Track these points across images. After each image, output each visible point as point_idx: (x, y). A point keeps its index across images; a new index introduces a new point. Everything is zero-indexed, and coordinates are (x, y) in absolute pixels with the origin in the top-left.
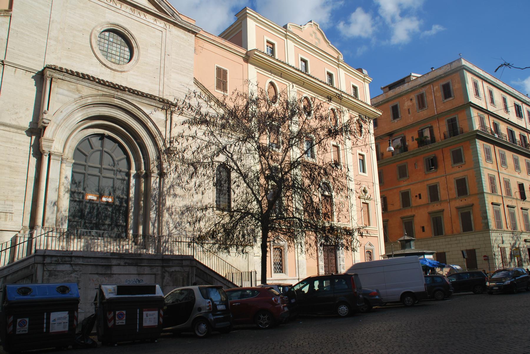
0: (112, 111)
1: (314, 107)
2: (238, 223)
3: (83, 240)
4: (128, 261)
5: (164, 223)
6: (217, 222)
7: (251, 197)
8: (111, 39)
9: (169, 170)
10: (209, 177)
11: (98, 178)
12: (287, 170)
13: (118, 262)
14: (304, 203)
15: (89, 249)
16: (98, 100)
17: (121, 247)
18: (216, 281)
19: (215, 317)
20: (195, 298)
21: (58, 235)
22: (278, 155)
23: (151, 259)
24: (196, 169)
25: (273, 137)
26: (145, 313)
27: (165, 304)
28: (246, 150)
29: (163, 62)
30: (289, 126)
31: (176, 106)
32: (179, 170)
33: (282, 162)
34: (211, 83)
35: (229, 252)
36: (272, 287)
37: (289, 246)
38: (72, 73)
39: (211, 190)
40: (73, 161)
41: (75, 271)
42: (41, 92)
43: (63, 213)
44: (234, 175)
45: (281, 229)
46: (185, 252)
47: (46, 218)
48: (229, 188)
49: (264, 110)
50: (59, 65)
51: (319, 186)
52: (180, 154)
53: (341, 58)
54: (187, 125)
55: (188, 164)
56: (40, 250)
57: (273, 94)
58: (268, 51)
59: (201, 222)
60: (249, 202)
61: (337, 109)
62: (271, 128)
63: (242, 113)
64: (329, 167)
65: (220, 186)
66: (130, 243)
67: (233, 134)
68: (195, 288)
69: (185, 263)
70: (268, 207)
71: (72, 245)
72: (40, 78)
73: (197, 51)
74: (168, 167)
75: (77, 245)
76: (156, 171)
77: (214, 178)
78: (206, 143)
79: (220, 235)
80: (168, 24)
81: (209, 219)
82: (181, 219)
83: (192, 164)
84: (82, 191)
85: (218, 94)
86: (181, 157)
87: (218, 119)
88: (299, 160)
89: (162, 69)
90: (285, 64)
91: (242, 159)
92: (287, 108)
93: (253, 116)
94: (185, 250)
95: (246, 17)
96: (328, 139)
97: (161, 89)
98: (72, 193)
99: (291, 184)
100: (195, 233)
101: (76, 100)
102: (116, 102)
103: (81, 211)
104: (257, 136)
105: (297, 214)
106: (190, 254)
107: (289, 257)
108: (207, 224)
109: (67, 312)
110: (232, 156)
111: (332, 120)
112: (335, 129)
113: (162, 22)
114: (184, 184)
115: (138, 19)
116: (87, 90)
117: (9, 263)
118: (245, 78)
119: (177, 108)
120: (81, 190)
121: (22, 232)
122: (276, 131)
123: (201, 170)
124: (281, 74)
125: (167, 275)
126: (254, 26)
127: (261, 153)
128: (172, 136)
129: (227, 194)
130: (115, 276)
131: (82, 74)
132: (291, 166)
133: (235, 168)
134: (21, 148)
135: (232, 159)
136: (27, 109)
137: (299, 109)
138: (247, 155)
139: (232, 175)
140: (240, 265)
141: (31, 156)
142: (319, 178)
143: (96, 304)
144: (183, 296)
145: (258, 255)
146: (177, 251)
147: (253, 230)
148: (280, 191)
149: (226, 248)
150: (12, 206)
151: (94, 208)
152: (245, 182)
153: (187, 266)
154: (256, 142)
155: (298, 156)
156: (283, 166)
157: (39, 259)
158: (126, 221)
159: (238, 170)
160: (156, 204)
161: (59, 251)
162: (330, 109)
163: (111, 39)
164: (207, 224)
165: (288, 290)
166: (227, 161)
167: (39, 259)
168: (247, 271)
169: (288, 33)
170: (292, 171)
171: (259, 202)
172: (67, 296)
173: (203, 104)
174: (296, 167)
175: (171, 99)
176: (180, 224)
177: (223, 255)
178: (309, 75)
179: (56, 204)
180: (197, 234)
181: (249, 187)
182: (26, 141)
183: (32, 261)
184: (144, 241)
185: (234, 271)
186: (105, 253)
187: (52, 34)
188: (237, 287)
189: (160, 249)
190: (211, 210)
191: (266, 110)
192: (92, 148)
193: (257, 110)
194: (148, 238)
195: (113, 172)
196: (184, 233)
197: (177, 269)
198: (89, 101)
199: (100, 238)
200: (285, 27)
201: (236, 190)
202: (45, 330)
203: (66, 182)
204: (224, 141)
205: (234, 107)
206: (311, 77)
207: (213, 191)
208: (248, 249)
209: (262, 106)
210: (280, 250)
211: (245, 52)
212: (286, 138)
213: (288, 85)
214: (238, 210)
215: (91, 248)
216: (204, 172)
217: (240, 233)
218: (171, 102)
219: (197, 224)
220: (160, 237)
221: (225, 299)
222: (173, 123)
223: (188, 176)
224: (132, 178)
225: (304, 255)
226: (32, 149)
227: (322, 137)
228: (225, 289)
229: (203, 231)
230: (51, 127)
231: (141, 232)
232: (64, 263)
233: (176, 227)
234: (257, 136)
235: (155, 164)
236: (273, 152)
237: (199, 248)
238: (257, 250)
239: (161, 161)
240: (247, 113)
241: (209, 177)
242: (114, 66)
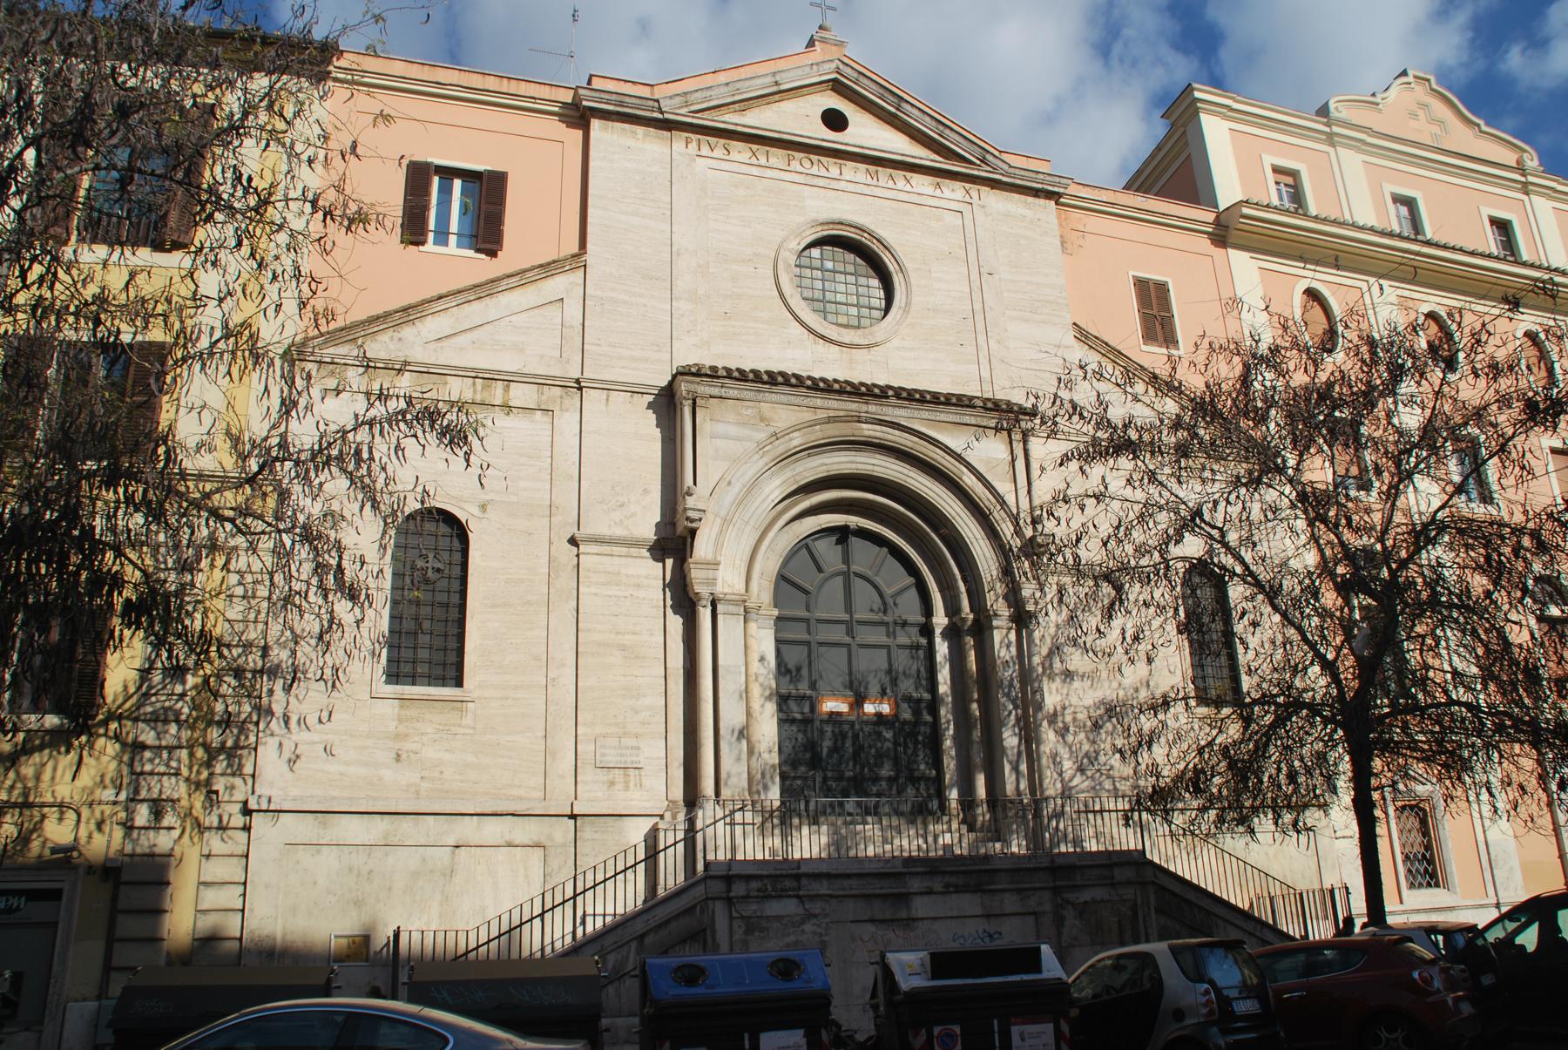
0: (859, 459)
1: (1463, 339)
2: (1269, 740)
3: (824, 828)
4: (953, 880)
5: (1044, 761)
6: (1203, 743)
7: (1300, 653)
8: (829, 265)
9: (1042, 604)
10: (1161, 609)
11: (885, 651)
12: (1403, 554)
13: (926, 884)
14: (1480, 651)
15: (843, 851)
16: (819, 434)
17: (930, 839)
18: (1220, 923)
19: (1231, 1039)
20: (1160, 981)
21: (758, 820)
22: (1368, 511)
23: (1019, 870)
24: (1119, 588)
25: (1343, 458)
26: (1015, 1030)
27: (1073, 1003)
28: (1264, 511)
29: (977, 296)
30: (1389, 415)
31: (1035, 415)
32: (1071, 600)
33: (1385, 531)
34: (1125, 329)
35: (1252, 831)
36: (1406, 934)
37: (1449, 798)
38: (742, 376)
39: (1173, 648)
40: (776, 612)
41: (810, 916)
42: (674, 440)
43: (766, 756)
44: (1237, 592)
45: (1413, 745)
46: (1116, 841)
47: (723, 775)
48: (1229, 636)
49: (1299, 379)
50: (379, 311)
51: (1525, 591)
52: (1068, 552)
53: (1532, 162)
54: (1074, 465)
55: (1095, 578)
56: (717, 863)
57: (1321, 324)
58: (1281, 199)
59: (1155, 747)
60: (1295, 671)
61: (1547, 331)
62: (1331, 431)
63: (1234, 401)
64: (1548, 525)
65: (1199, 631)
66: (955, 825)
67: (1216, 467)
68: (1159, 948)
69: (1120, 874)
70: (1359, 677)
71: (797, 843)
72: (667, 403)
73: (1068, 245)
74: (1038, 594)
75: (809, 844)
76: (1003, 610)
77: (1176, 610)
78: (1137, 508)
79: (1217, 780)
80: (974, 189)
81: (1179, 736)
82: (1094, 742)
83: (1107, 577)
84: (808, 692)
85: (1153, 357)
86: (1071, 561)
87: (1165, 432)
88: (1440, 515)
89: (979, 317)
90: (1343, 224)
91: (1255, 539)
92: (1375, 360)
93: (1270, 403)
94: (1116, 835)
95: (1196, 112)
96: (1531, 434)
97: (986, 374)
98: (783, 700)
99: (1424, 595)
100: (1142, 783)
101: (761, 447)
102: (867, 433)
103: (812, 746)
104: (1291, 463)
105: (1461, 690)
106: (1132, 847)
107: (1457, 831)
108: (1175, 752)
109: (801, 1032)
110: (1223, 535)
111: (1535, 370)
112: (1547, 398)
113: (958, 185)
114: (1089, 640)
115: (890, 194)
116: (785, 412)
117: (645, 901)
118: (1225, 295)
119: (1038, 421)
120: (804, 688)
121: (668, 816)
122: (1347, 435)
123: (1134, 591)
124: (1337, 258)
125: (1069, 914)
126: (1227, 134)
127: (1312, 515)
128: (1036, 502)
129: (1224, 652)
131: (767, 372)
132: (1417, 538)
133: (1239, 570)
134: (642, 593)
135: (1226, 545)
136: (646, 491)
137: (1414, 357)
138: (1270, 525)
139: (1231, 593)
140: (1296, 867)
141: (669, 611)
142: (1520, 565)
143: (875, 1007)
144: (1125, 976)
145: (1348, 833)
146: (1094, 841)
147: (1321, 757)
148: (1393, 624)
149: (1243, 820)
150: (638, 748)
151: (844, 736)
152: (1275, 608)
153: (1128, 883)
154: (1291, 481)
155: (1436, 503)
156: (1389, 543)
157: (717, 888)
158: (937, 763)
159: (1250, 577)
160: (1016, 707)
161: (764, 861)
162: (1520, 334)
163: (829, 265)
164: (1175, 752)
165: (1464, 944)
166: (1211, 552)
167: (717, 888)
168: (1317, 886)
169: (1336, 129)
170: (1424, 554)
171: (1329, 667)
172: (796, 985)
173: (1113, 395)
174: (1433, 541)
175: (1018, 398)
176: (1092, 758)
177: (1234, 842)
178: (1428, 243)
179: (743, 733)
180: (1147, 783)
181: (1292, 624)
182: (652, 574)
183: (699, 891)
184: (994, 819)
185: (1276, 890)
186: (888, 861)
187: (680, 285)
188: (1293, 939)
189: (1043, 837)
190: (1180, 706)
191: (1308, 379)
192: (820, 570)
193: (1280, 383)
194: (1004, 809)
195: (883, 629)
196: (1108, 785)
197: (1099, 893)
198: (795, 443)
199: (869, 819)
200: (1323, 111)
201: (1250, 639)
203: (764, 671)
204: (1191, 493)
205: (1207, 386)
206: (1437, 246)
207: (1178, 647)
208: (1312, 816)
209: (1292, 368)
210: (1421, 816)
211: (1211, 217)
212: (1386, 452)
213: (1365, 289)
214: (1266, 699)
215: (848, 849)
216: (1146, 596)
217: (1279, 770)
218: (1020, 406)
219: (1145, 755)
220: (1038, 803)
221: (1255, 981)
222: (1035, 466)
223: (1099, 613)
224: (938, 639)
225: (1503, 823)
226: (668, 594)
227: (1510, 431)
228: (1251, 948)
229: (1165, 773)
230: (707, 530)
231: (981, 792)
232: (781, 895)
233: (1081, 770)
234: (1291, 463)
235: (999, 591)
236: (1350, 505)
237: (1158, 826)
238: (1341, 818)
239: (1013, 581)
240: (1249, 400)
241: (1161, 609)
242: (848, 336)
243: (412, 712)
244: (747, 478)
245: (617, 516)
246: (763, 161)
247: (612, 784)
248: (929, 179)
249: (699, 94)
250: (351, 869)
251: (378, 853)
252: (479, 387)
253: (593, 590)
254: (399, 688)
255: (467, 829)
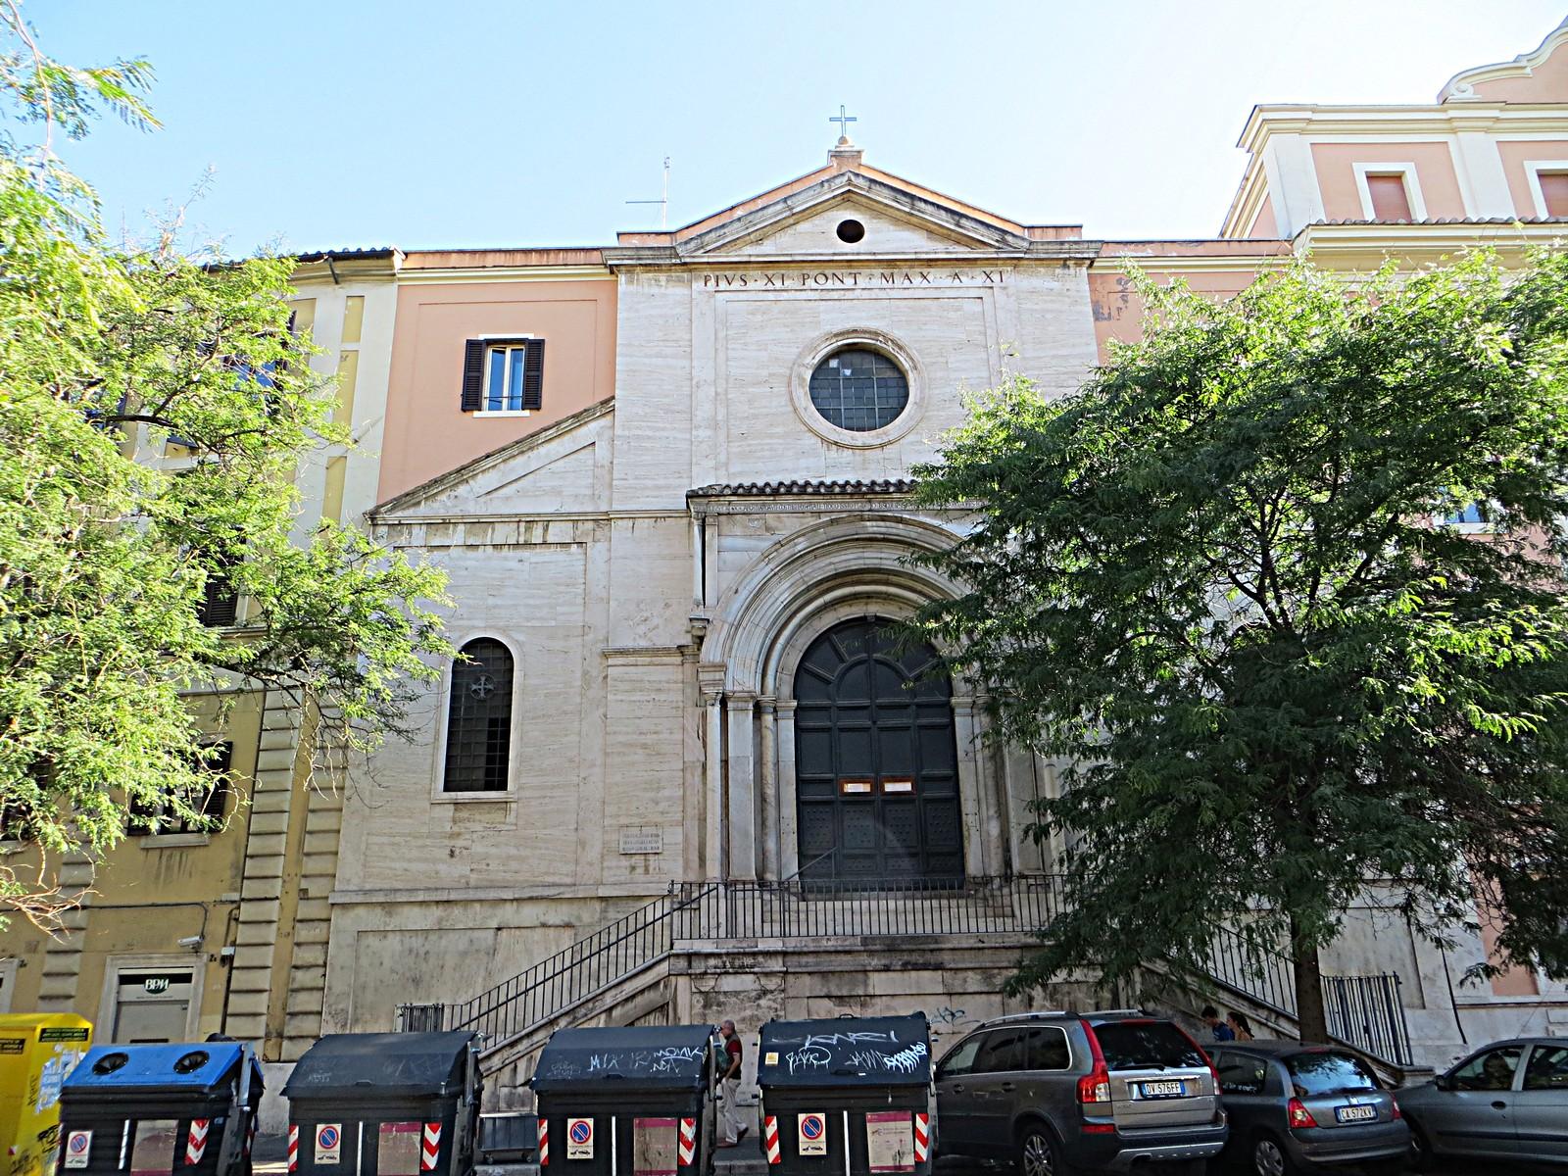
38: (748, 491)
102: (871, 530)
113: (977, 271)
116: (789, 521)
130: (877, 1000)
134: (663, 697)
198: (799, 548)
202: (121, 1165)
232: (740, 971)
243: (464, 814)
244: (753, 585)
245: (642, 629)
246: (778, 285)
247: (633, 868)
248: (947, 271)
249: (713, 235)
250: (411, 951)
251: (433, 937)
252: (522, 529)
253: (619, 697)
254: (453, 795)
255: (508, 914)
